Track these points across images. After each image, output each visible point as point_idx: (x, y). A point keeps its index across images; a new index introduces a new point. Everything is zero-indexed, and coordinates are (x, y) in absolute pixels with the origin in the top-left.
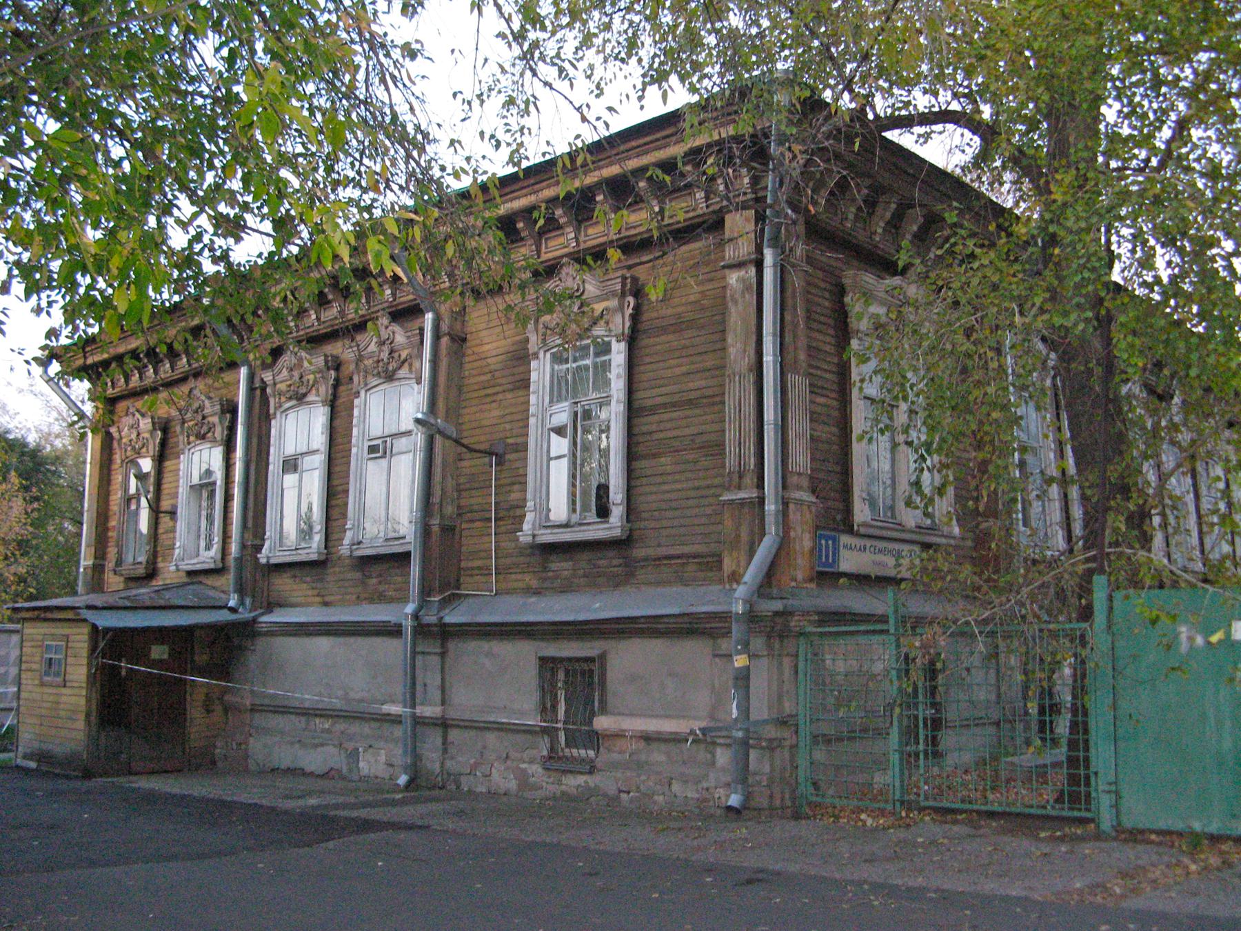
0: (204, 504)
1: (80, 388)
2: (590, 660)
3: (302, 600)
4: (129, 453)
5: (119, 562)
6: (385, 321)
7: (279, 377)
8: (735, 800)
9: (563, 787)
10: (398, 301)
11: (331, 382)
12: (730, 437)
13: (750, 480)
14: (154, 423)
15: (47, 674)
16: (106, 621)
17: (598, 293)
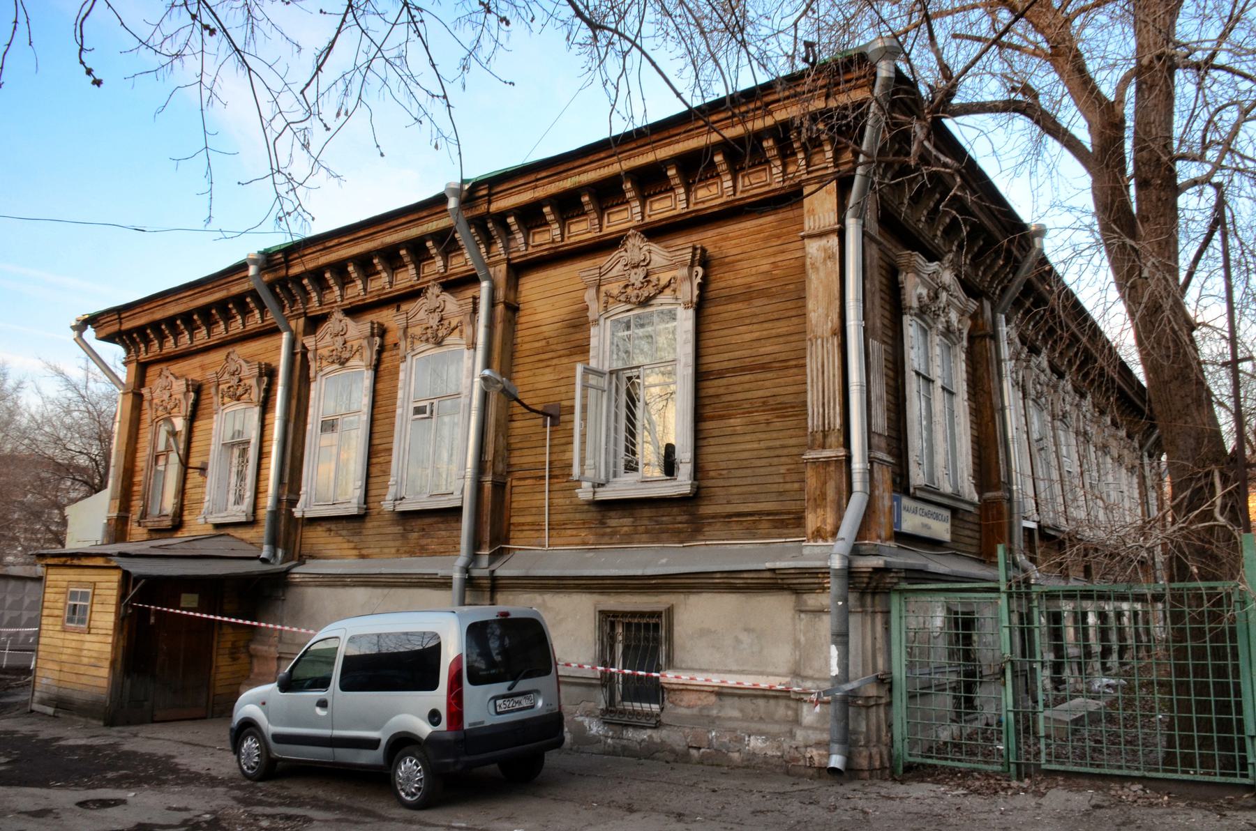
0: (235, 461)
1: (114, 353)
2: (657, 614)
3: (337, 553)
4: (159, 413)
5: (144, 515)
6: (437, 290)
7: (322, 343)
8: (836, 761)
9: (625, 742)
10: (449, 272)
11: (376, 348)
12: (812, 398)
13: (836, 438)
14: (188, 385)
15: (70, 620)
16: (139, 568)
17: (665, 263)
